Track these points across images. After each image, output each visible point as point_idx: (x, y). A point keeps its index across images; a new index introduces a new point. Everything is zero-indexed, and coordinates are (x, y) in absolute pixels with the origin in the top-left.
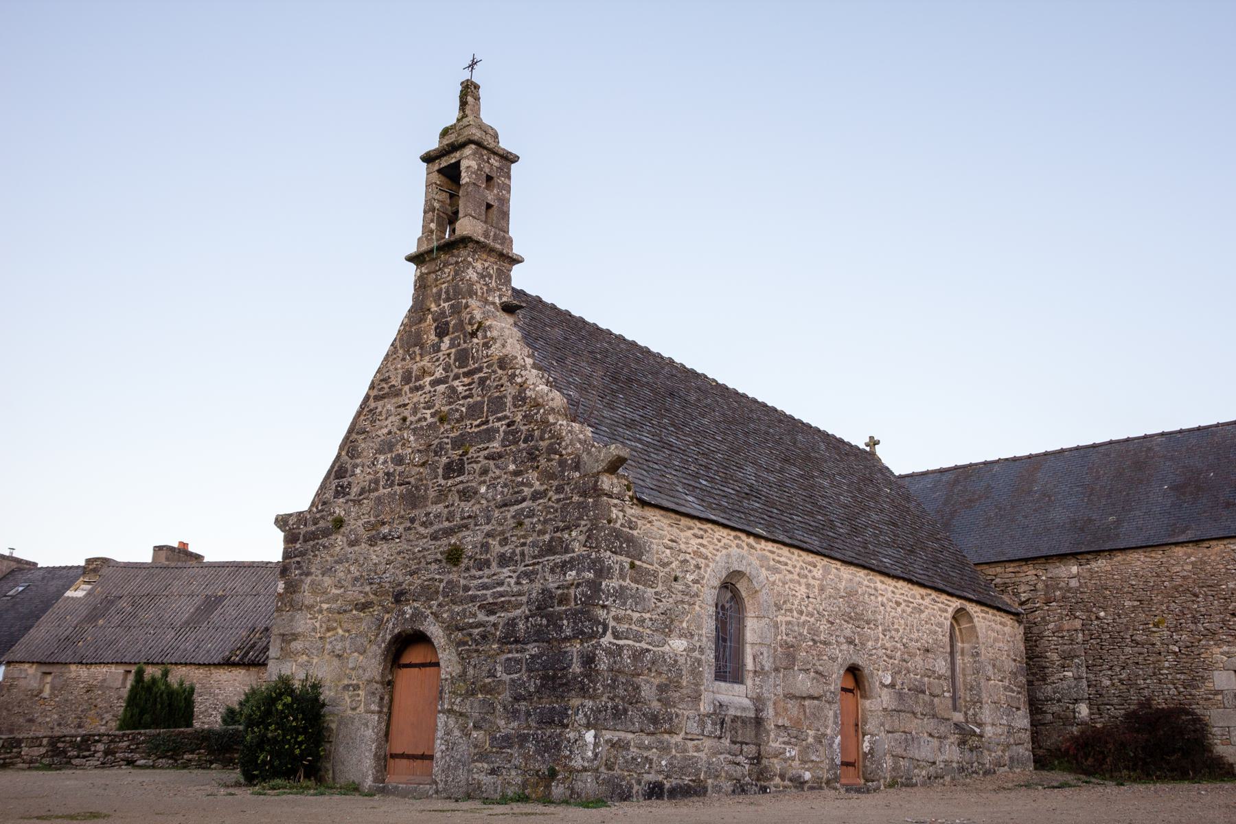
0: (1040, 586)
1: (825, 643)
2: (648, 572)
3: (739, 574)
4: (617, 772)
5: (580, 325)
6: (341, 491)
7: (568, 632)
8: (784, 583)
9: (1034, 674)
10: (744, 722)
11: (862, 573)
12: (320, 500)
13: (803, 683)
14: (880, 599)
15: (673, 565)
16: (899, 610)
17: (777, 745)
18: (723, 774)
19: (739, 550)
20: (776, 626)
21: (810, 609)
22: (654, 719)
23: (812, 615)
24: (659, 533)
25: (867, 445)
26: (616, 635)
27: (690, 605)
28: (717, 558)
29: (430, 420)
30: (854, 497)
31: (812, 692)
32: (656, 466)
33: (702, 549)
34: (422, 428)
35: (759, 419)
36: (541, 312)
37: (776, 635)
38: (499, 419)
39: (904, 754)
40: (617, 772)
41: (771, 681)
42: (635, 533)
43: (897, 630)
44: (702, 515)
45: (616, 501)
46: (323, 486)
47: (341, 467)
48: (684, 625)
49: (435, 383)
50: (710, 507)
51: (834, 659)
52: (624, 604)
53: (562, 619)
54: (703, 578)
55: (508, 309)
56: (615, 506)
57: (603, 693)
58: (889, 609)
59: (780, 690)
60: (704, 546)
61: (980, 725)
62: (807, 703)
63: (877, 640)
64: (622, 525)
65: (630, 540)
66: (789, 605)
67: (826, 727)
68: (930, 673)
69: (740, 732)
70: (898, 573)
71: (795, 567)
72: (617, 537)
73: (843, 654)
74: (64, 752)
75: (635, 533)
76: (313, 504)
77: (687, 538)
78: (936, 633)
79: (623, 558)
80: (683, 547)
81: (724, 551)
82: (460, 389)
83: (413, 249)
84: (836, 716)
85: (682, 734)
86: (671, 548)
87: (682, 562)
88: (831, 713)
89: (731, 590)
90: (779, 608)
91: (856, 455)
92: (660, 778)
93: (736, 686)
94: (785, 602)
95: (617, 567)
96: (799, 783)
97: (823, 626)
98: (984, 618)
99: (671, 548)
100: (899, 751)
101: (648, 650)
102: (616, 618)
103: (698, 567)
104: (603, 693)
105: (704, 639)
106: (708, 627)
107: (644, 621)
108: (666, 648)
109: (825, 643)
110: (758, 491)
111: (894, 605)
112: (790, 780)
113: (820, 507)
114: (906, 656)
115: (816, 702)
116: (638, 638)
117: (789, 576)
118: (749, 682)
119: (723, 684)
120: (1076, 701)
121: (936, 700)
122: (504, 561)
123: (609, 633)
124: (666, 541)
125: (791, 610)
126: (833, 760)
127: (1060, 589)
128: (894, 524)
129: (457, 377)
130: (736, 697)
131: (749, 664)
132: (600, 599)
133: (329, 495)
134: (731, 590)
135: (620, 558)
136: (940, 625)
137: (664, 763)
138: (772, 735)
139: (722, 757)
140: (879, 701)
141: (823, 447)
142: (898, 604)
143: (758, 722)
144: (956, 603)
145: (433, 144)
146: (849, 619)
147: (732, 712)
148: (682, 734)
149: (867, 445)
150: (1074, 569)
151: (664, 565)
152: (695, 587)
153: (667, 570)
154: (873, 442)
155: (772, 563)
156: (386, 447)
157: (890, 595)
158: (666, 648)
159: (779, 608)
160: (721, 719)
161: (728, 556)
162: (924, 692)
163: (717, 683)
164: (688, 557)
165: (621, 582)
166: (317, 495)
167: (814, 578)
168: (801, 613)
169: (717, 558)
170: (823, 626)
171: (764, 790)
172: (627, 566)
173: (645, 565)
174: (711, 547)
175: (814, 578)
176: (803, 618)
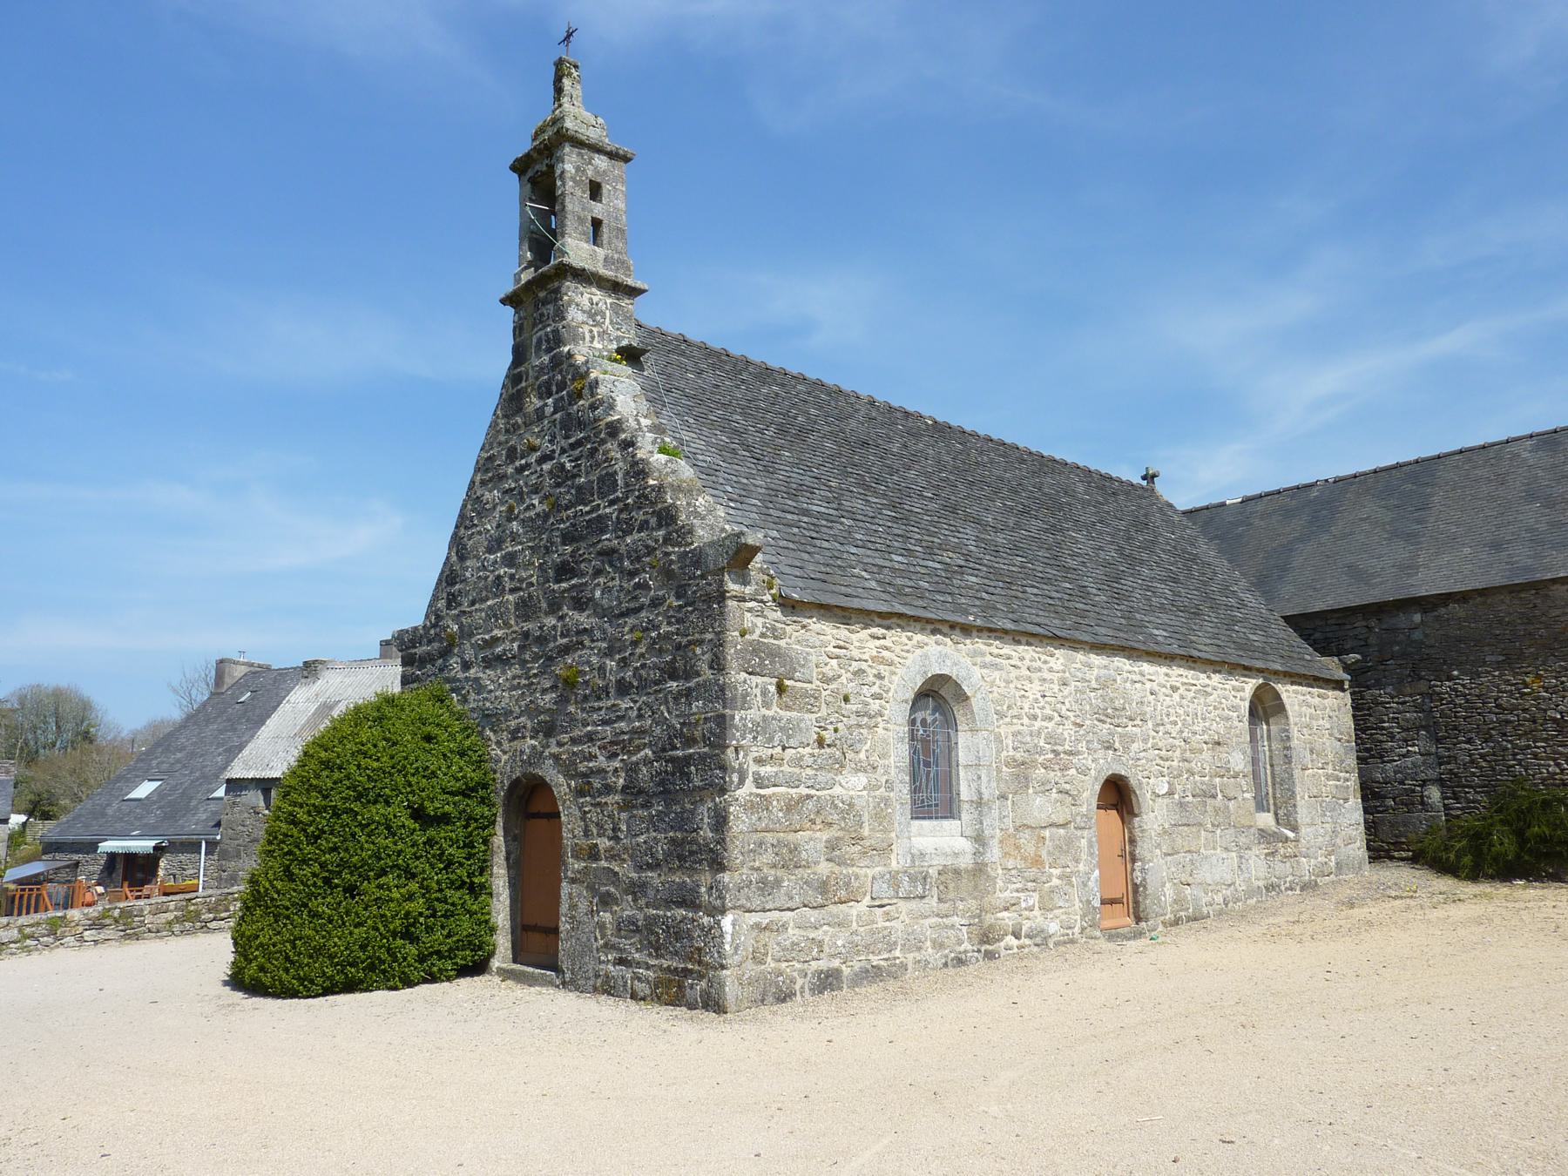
0: (1373, 640)
1: (1070, 753)
2: (805, 694)
3: (943, 679)
4: (771, 964)
5: (741, 365)
6: (452, 601)
7: (697, 782)
8: (1008, 682)
9: (1367, 750)
10: (957, 872)
11: (1121, 662)
12: (434, 615)
13: (1041, 807)
14: (1148, 685)
15: (843, 679)
16: (1176, 696)
17: (1007, 894)
18: (928, 943)
19: (940, 648)
20: (998, 739)
21: (1048, 711)
22: (823, 887)
23: (1051, 719)
24: (816, 642)
25: (1144, 478)
26: (759, 782)
27: (870, 728)
28: (908, 662)
29: (539, 508)
30: (1120, 550)
31: (1054, 818)
32: (826, 545)
33: (885, 653)
34: (531, 519)
35: (992, 462)
36: (683, 354)
37: (999, 752)
38: (612, 503)
39: (1190, 880)
40: (771, 964)
41: (995, 813)
42: (782, 643)
43: (1175, 723)
44: (884, 608)
45: (752, 604)
46: (435, 598)
47: (452, 571)
48: (862, 756)
49: (541, 461)
50: (899, 593)
51: (1084, 772)
52: (771, 739)
53: (688, 765)
54: (887, 692)
55: (631, 355)
56: (750, 610)
57: (743, 863)
58: (1161, 698)
59: (1008, 822)
60: (887, 649)
61: (1294, 829)
62: (1047, 833)
63: (1145, 741)
64: (763, 635)
65: (775, 653)
66: (1015, 712)
67: (1077, 861)
68: (1224, 771)
69: (951, 886)
70: (1175, 649)
71: (1021, 659)
72: (755, 652)
73: (1096, 768)
74: (198, 914)
75: (782, 643)
76: (427, 616)
77: (860, 641)
78: (1228, 719)
79: (766, 679)
80: (856, 653)
81: (919, 651)
82: (568, 466)
83: (509, 288)
84: (1090, 845)
85: (867, 900)
86: (838, 657)
87: (855, 674)
88: (1084, 842)
89: (938, 696)
90: (1001, 715)
91: (1127, 494)
92: (836, 963)
93: (946, 823)
94: (1009, 707)
95: (758, 691)
96: (1041, 938)
97: (1068, 731)
98: (1296, 692)
99: (838, 657)
100: (1185, 877)
101: (809, 797)
102: (759, 761)
103: (879, 677)
104: (743, 863)
105: (893, 771)
106: (898, 754)
107: (801, 758)
108: (837, 790)
109: (1070, 753)
110: (979, 561)
111: (1169, 691)
112: (1028, 936)
113: (1068, 569)
114: (1188, 755)
115: (1062, 831)
116: (793, 782)
117: (1014, 673)
118: (964, 816)
119: (926, 823)
120: (1424, 783)
121: (1231, 804)
122: (623, 689)
123: (749, 781)
124: (830, 648)
125: (1018, 717)
126: (1089, 902)
127: (1398, 643)
128: (1176, 581)
129: (563, 451)
130: (941, 840)
131: (965, 792)
132: (734, 737)
133: (441, 604)
134: (938, 696)
135: (759, 680)
136: (1234, 708)
137: (840, 943)
138: (1000, 883)
139: (927, 922)
140: (1154, 816)
141: (1080, 488)
142: (1174, 689)
143: (979, 870)
144: (1251, 685)
145: (524, 146)
146: (1102, 715)
147: (938, 862)
148: (867, 900)
149: (1144, 478)
150: (1417, 618)
151: (827, 680)
152: (875, 705)
153: (833, 686)
154: (1150, 477)
155: (988, 658)
156: (495, 545)
157: (1162, 679)
158: (837, 790)
159: (1001, 715)
160: (920, 881)
161: (926, 656)
162: (1214, 797)
163: (917, 823)
164: (864, 666)
165: (764, 711)
166: (430, 606)
167: (1051, 670)
168: (1035, 718)
169: (908, 662)
170: (1068, 731)
171: (990, 956)
172: (773, 689)
173: (799, 684)
174: (898, 649)
175: (1051, 670)
176: (1038, 724)
